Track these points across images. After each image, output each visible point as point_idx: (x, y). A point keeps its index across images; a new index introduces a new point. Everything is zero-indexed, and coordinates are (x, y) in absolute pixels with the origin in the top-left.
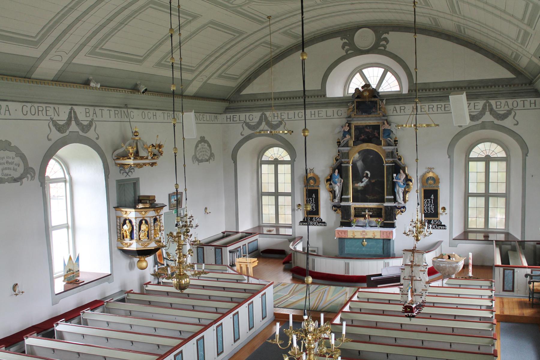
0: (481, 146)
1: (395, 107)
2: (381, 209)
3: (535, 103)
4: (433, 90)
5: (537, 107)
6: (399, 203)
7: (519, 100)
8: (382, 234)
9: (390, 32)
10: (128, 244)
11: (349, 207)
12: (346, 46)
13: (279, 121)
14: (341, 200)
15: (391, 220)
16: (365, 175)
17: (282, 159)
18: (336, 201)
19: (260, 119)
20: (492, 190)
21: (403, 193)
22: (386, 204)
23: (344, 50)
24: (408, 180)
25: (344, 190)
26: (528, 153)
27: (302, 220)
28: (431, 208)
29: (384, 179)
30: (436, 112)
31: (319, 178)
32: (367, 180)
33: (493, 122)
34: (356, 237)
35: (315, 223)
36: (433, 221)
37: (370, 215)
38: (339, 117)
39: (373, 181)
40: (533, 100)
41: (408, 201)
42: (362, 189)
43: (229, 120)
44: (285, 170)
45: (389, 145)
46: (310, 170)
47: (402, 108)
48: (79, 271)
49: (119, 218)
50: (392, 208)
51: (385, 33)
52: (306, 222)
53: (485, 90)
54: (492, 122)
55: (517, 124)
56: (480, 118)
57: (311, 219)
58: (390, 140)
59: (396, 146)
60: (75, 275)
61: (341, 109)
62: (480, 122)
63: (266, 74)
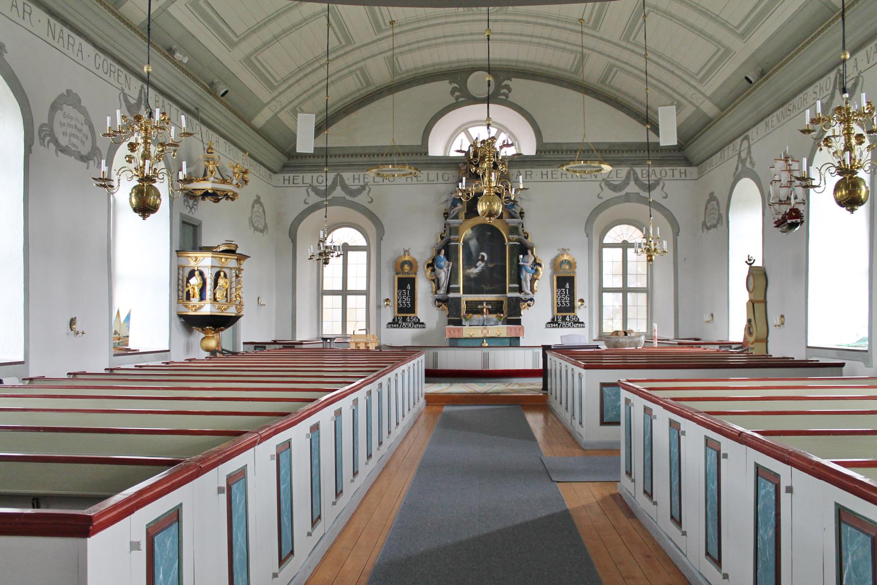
1: (519, 172)
2: (502, 302)
4: (567, 152)
6: (526, 294)
7: (667, 169)
8: (509, 331)
9: (512, 79)
10: (198, 306)
11: (459, 299)
12: (456, 91)
13: (361, 186)
14: (449, 290)
15: (516, 316)
16: (480, 257)
18: (442, 291)
21: (530, 281)
22: (509, 295)
23: (453, 96)
25: (453, 277)
27: (391, 321)
28: (565, 300)
29: (506, 263)
30: (570, 179)
32: (483, 264)
33: (639, 193)
34: (474, 336)
35: (410, 325)
36: (568, 317)
37: (489, 309)
38: (445, 182)
40: (683, 169)
41: (536, 291)
44: (358, 261)
45: (513, 217)
46: (405, 251)
47: (528, 173)
48: (128, 337)
49: (181, 267)
50: (518, 300)
51: (508, 79)
55: (666, 197)
56: (623, 189)
57: (564, 318)
58: (514, 211)
59: (522, 219)
62: (623, 193)
63: (344, 122)
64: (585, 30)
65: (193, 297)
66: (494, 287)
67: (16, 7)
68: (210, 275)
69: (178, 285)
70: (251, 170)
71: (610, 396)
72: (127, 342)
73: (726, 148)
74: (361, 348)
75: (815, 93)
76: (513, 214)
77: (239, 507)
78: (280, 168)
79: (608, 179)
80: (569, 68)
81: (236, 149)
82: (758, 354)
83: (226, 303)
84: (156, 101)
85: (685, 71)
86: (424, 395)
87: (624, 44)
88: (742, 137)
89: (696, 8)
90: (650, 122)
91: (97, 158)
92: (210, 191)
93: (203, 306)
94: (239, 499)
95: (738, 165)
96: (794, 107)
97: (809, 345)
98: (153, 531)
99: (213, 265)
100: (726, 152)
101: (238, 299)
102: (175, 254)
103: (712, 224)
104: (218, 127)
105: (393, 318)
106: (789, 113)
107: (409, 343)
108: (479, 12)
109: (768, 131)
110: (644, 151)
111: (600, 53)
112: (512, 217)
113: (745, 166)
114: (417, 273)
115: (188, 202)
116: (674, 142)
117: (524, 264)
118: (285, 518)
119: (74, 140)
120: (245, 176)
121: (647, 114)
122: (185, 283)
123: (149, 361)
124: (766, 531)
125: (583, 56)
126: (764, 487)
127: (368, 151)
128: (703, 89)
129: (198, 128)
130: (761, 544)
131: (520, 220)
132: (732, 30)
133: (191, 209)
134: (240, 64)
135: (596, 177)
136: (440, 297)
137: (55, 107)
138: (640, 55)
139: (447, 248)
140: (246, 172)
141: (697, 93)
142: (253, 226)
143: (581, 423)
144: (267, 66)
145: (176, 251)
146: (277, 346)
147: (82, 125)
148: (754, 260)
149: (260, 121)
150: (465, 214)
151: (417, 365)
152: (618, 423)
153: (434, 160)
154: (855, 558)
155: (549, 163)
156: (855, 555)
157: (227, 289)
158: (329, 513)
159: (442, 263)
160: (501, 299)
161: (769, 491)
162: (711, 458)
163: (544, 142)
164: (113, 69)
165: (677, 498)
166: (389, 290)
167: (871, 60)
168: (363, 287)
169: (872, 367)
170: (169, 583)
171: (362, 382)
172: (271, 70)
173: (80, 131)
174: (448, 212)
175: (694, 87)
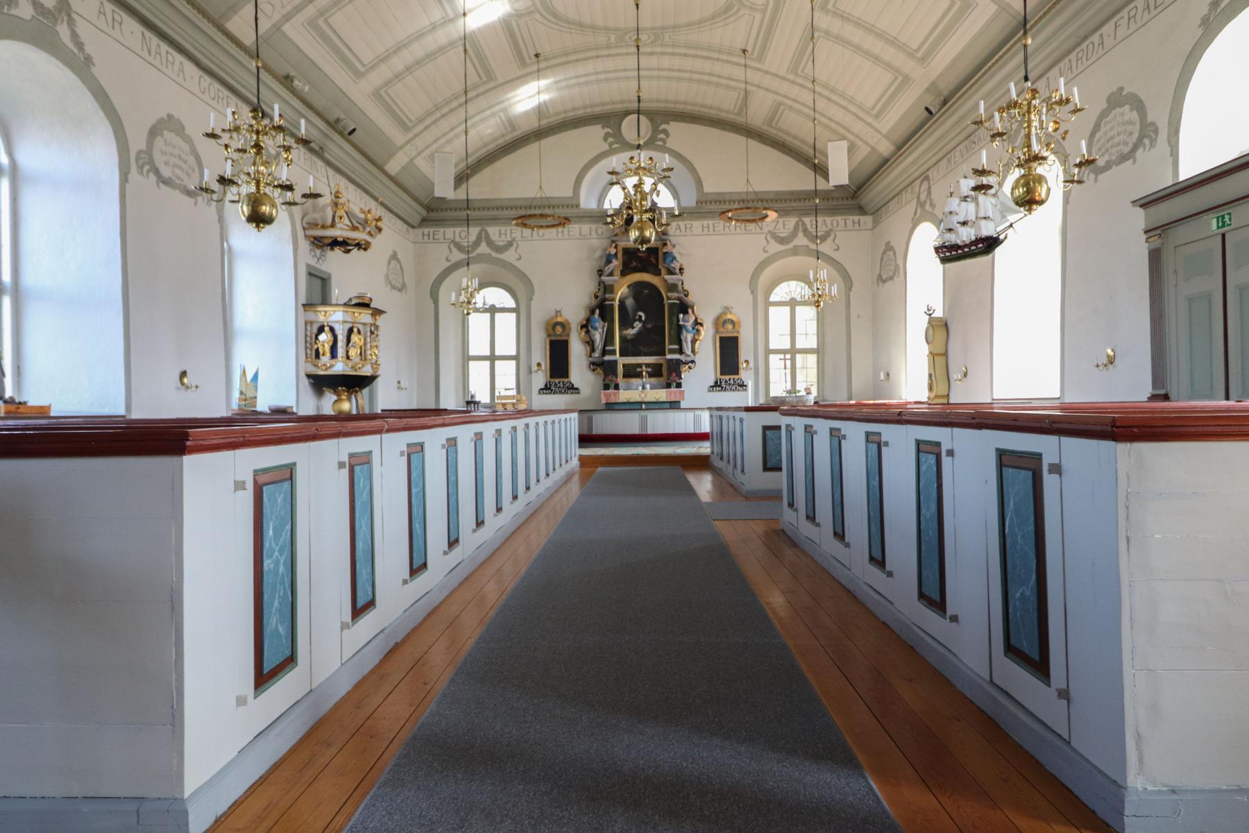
0: (784, 286)
2: (661, 365)
5: (862, 227)
6: (687, 355)
7: (839, 218)
11: (616, 362)
13: (509, 242)
14: (604, 353)
16: (637, 317)
17: (502, 306)
18: (597, 354)
20: (800, 344)
21: (692, 342)
22: (669, 357)
24: (697, 323)
25: (609, 339)
26: (852, 286)
31: (569, 324)
35: (563, 391)
39: (649, 326)
40: (856, 218)
42: (633, 337)
43: (426, 238)
44: (507, 323)
47: (688, 226)
48: (255, 398)
50: (679, 362)
54: (805, 246)
55: (838, 249)
56: (791, 241)
60: (248, 404)
62: (791, 246)
64: (749, 62)
65: (323, 355)
66: (652, 349)
67: (105, 15)
68: (341, 331)
69: (306, 342)
71: (772, 439)
72: (254, 404)
76: (672, 269)
78: (418, 222)
79: (774, 231)
80: (732, 109)
83: (360, 362)
85: (860, 107)
86: (577, 457)
87: (791, 77)
88: (922, 178)
92: (339, 239)
93: (334, 365)
100: (904, 196)
101: (374, 357)
102: (301, 308)
111: (767, 90)
112: (671, 272)
115: (315, 252)
116: (845, 181)
117: (685, 324)
119: (178, 172)
120: (379, 224)
122: (314, 340)
128: (878, 126)
129: (324, 170)
131: (679, 276)
132: (911, 55)
133: (318, 260)
134: (368, 98)
135: (761, 229)
136: (595, 360)
137: (153, 133)
139: (601, 308)
140: (379, 219)
142: (390, 283)
143: (743, 471)
144: (398, 101)
145: (303, 305)
147: (187, 155)
148: (934, 310)
149: (393, 167)
150: (621, 271)
152: (780, 469)
153: (586, 213)
155: (709, 215)
157: (361, 347)
159: (597, 324)
160: (661, 362)
164: (221, 94)
165: (840, 509)
166: (540, 355)
172: (402, 107)
173: (185, 162)
174: (603, 269)
175: (870, 125)
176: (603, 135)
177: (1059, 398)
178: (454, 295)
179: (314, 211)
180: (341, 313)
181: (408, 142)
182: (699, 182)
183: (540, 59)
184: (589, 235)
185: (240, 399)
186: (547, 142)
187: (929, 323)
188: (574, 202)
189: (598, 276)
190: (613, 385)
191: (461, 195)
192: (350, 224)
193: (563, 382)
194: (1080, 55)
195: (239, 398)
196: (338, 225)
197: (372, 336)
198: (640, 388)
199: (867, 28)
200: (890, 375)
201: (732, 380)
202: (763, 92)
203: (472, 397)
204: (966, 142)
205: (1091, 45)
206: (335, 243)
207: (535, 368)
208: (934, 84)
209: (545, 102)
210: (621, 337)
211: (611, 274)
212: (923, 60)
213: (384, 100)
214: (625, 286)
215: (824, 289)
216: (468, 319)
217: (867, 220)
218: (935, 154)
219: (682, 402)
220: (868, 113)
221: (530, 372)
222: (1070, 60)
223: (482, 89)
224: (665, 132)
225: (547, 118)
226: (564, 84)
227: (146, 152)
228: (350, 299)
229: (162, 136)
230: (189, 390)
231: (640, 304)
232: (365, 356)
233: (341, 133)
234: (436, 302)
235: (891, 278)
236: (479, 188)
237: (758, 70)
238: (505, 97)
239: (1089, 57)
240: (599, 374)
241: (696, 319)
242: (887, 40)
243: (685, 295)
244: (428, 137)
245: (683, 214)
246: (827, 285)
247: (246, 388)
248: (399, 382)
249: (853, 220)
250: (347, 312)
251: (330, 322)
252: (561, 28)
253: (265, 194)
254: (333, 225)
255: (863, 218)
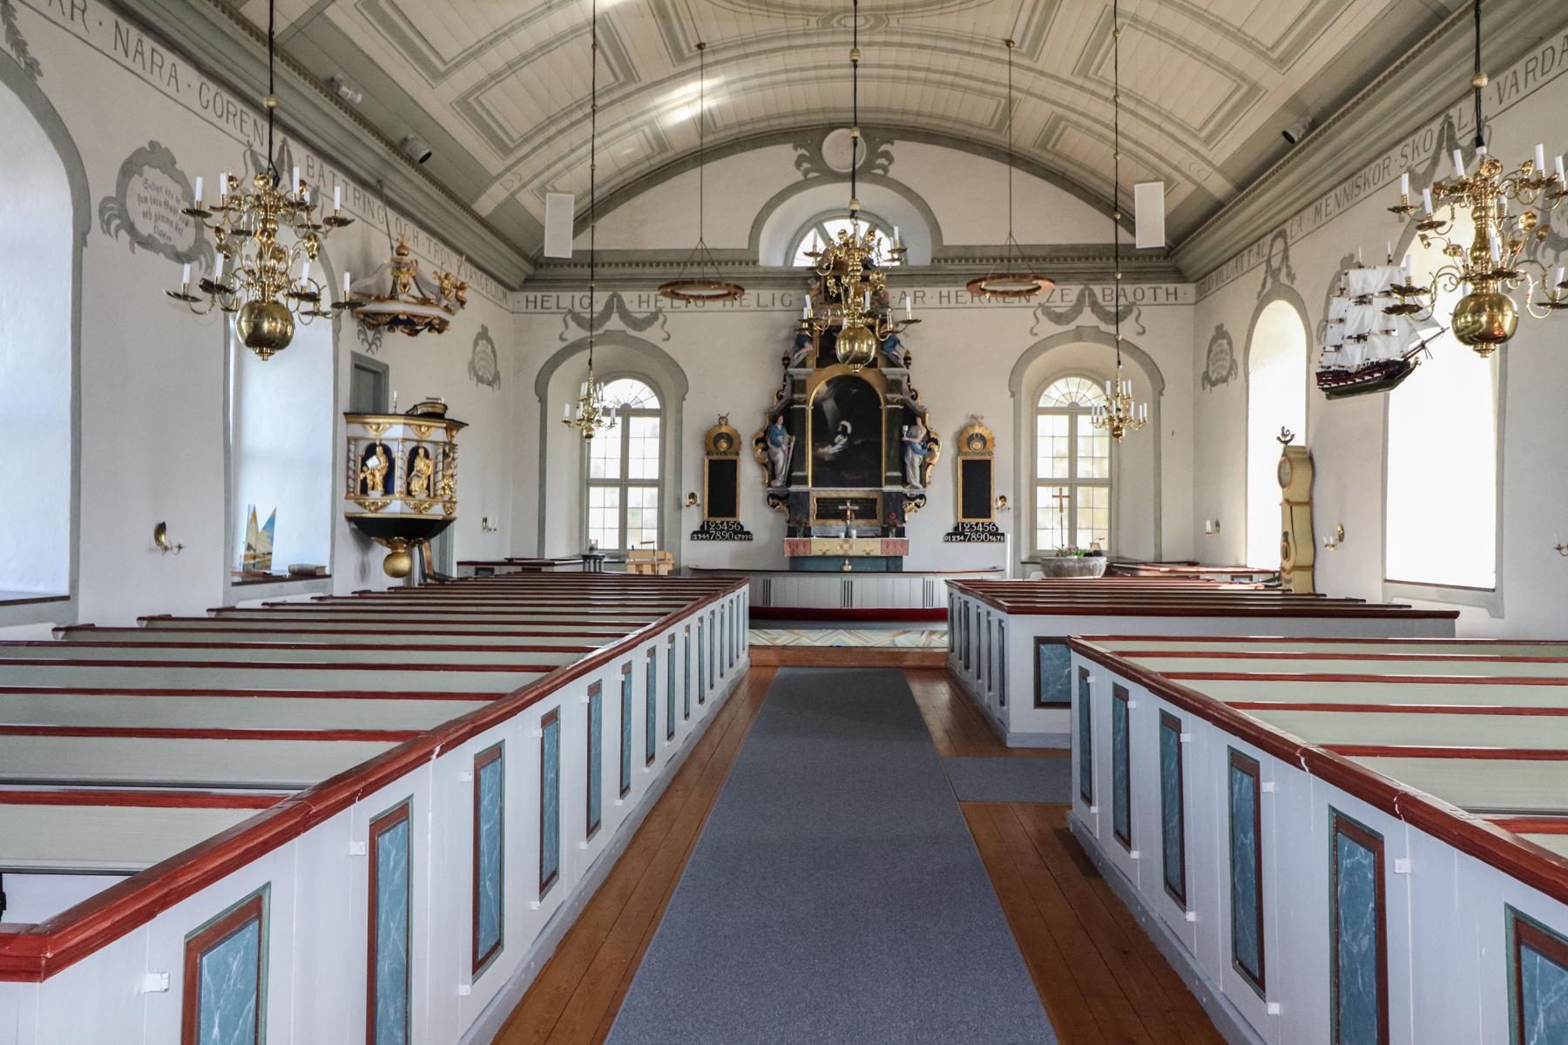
2: (875, 500)
3: (1176, 293)
5: (1180, 301)
7: (1145, 287)
8: (885, 546)
11: (808, 493)
13: (652, 313)
14: (790, 480)
16: (840, 429)
17: (639, 406)
19: (606, 306)
21: (921, 467)
22: (887, 488)
24: (930, 440)
25: (797, 460)
27: (698, 529)
29: (881, 438)
30: (986, 304)
32: (844, 440)
33: (1097, 327)
34: (829, 553)
35: (728, 535)
39: (858, 442)
40: (1171, 287)
43: (531, 305)
44: (645, 431)
47: (918, 294)
48: (270, 554)
50: (902, 497)
51: (887, 142)
52: (707, 532)
53: (1081, 265)
56: (1073, 320)
59: (908, 368)
61: (792, 292)
62: (1072, 326)
63: (623, 211)
64: (1015, 59)
65: (373, 489)
69: (348, 468)
70: (471, 283)
71: (1049, 658)
73: (1246, 252)
74: (645, 573)
75: (1404, 156)
76: (893, 358)
77: (393, 874)
81: (446, 249)
82: (1298, 592)
84: (308, 166)
87: (1079, 81)
88: (1275, 233)
89: (1200, 16)
90: (1118, 209)
91: (205, 256)
92: (401, 317)
94: (395, 859)
95: (1265, 279)
96: (1366, 181)
97: (1388, 578)
98: (199, 945)
99: (407, 437)
100: (1246, 258)
101: (447, 492)
102: (342, 419)
103: (1219, 376)
104: (412, 209)
105: (701, 524)
106: (1356, 191)
107: (725, 565)
108: (843, 29)
109: (1319, 224)
110: (1108, 259)
112: (892, 363)
113: (1279, 280)
114: (741, 452)
116: (1160, 242)
118: (488, 883)
119: (163, 226)
120: (460, 293)
121: (1116, 198)
123: (288, 594)
124: (1354, 938)
125: (1010, 101)
126: (1351, 854)
127: (659, 258)
129: (382, 213)
130: (1345, 959)
131: (904, 370)
132: (1263, 55)
136: (776, 491)
137: (129, 169)
138: (1106, 99)
139: (786, 414)
140: (461, 287)
141: (1199, 161)
142: (476, 374)
145: (345, 414)
146: (513, 569)
147: (178, 201)
148: (1293, 436)
149: (485, 205)
151: (742, 596)
154: (1553, 1019)
156: (1553, 1014)
157: (429, 476)
158: (664, 749)
159: (780, 438)
161: (1359, 862)
162: (1240, 788)
163: (945, 243)
164: (232, 110)
166: (694, 480)
167: (1505, 99)
168: (654, 474)
169: (1503, 617)
170: (234, 1041)
171: (640, 635)
175: (1195, 152)
176: (794, 159)
177: (1494, 590)
178: (568, 407)
179: (367, 275)
180: (401, 427)
181: (508, 169)
182: (936, 230)
183: (704, 51)
184: (770, 304)
185: (246, 557)
186: (711, 168)
187: (1284, 454)
188: (752, 257)
189: (783, 367)
190: (802, 530)
191: (584, 243)
192: (420, 296)
193: (728, 523)
194: (1531, 65)
195: (245, 556)
196: (403, 297)
197: (446, 461)
198: (843, 535)
199: (1195, 14)
200: (1221, 524)
201: (980, 525)
202: (1034, 100)
203: (592, 549)
204: (1346, 185)
205: (1550, 51)
206: (394, 322)
207: (686, 500)
208: (1296, 98)
209: (710, 111)
210: (814, 458)
211: (803, 364)
212: (1281, 62)
213: (474, 111)
214: (823, 382)
215: (1128, 410)
216: (589, 444)
217: (1187, 291)
218: (1298, 199)
219: (905, 558)
220: (1195, 136)
221: (680, 507)
222: (1515, 72)
223: (618, 94)
224: (887, 155)
225: (714, 133)
226: (739, 85)
227: (115, 199)
228: (415, 407)
229: (141, 175)
230: (168, 552)
231: (844, 409)
232: (435, 491)
233: (409, 160)
234: (543, 401)
235: (1224, 380)
236: (611, 234)
237: (1029, 69)
238: (651, 105)
239: (1545, 70)
240: (780, 511)
241: (928, 432)
242: (1227, 32)
243: (912, 397)
244: (537, 162)
245: (906, 276)
246: (1133, 403)
247: (257, 539)
248: (485, 520)
249: (1167, 289)
250: (410, 425)
251: (385, 439)
252: (735, 8)
253: (276, 303)
254: (393, 297)
255: (1181, 287)
